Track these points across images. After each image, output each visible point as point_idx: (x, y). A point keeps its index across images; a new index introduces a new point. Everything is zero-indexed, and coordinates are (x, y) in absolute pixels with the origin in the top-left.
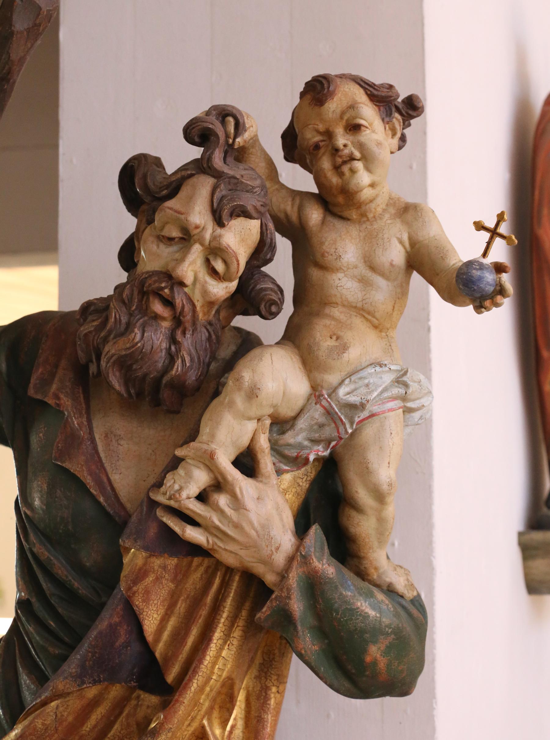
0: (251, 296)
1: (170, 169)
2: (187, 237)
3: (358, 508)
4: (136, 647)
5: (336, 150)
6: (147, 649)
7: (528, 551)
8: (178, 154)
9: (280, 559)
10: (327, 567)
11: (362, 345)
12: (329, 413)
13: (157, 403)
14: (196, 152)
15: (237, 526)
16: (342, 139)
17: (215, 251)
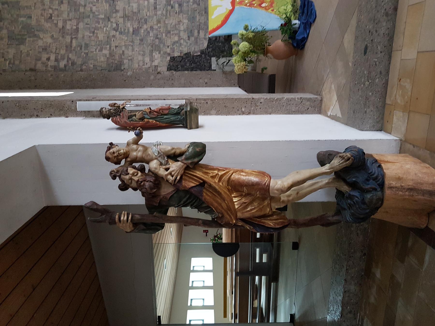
0: (142, 169)
1: (120, 183)
2: (131, 179)
3: (175, 152)
4: (197, 187)
5: (117, 156)
6: (197, 186)
7: (191, 128)
8: (118, 182)
9: (182, 164)
10: (184, 157)
11: (150, 152)
12: (159, 157)
13: (158, 184)
14: (117, 178)
15: (177, 171)
16: (116, 155)
17: (133, 174)
